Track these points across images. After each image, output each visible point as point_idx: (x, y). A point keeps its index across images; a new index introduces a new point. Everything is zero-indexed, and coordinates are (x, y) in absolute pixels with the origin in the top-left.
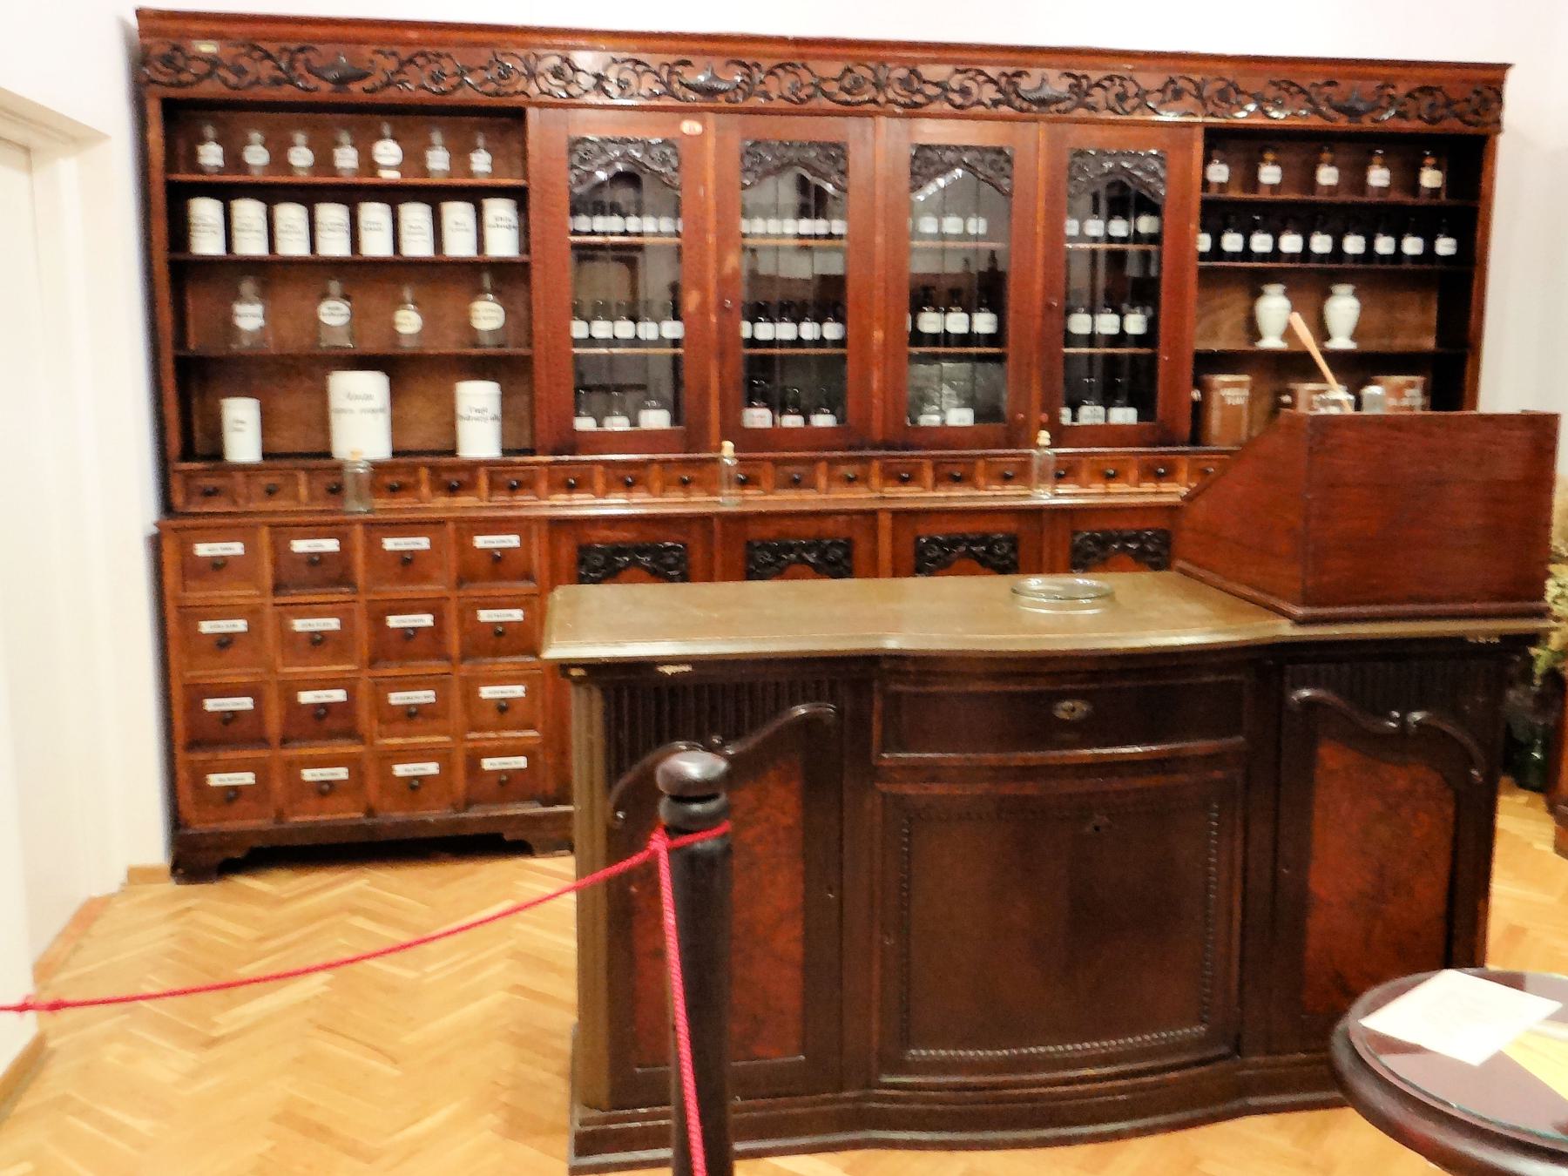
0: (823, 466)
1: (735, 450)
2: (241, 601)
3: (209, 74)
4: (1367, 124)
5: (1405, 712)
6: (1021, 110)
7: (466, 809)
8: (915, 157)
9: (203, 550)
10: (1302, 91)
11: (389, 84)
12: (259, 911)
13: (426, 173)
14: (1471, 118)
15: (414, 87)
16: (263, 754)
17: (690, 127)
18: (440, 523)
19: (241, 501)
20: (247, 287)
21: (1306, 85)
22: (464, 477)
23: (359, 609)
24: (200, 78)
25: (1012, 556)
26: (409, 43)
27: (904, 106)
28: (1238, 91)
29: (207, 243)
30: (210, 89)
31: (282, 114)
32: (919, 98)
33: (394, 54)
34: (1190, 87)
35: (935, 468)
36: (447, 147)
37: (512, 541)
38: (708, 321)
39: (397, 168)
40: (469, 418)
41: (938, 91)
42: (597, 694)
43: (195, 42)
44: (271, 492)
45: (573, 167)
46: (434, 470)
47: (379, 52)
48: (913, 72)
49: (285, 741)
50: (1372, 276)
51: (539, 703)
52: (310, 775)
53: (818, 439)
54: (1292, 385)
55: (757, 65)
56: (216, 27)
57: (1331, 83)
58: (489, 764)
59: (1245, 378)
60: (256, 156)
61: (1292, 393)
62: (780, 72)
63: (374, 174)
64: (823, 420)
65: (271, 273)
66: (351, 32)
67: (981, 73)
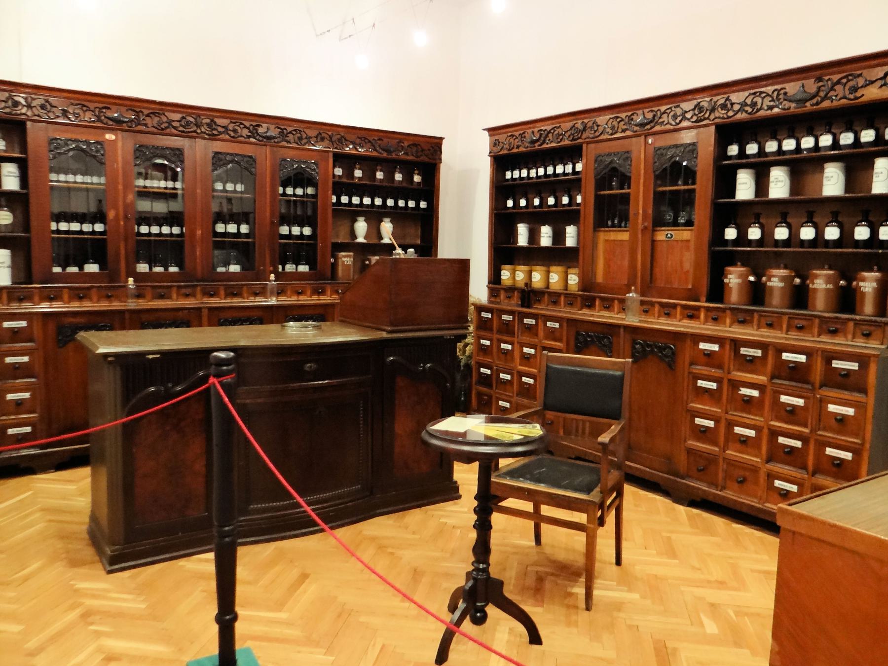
0: (174, 290)
1: (134, 281)
4: (394, 156)
5: (425, 364)
10: (370, 142)
17: (110, 136)
27: (209, 135)
32: (215, 132)
37: (24, 324)
38: (119, 224)
42: (118, 368)
48: (212, 120)
50: (396, 215)
53: (167, 276)
57: (379, 139)
59: (351, 254)
61: (370, 260)
64: (173, 269)
67: (242, 124)
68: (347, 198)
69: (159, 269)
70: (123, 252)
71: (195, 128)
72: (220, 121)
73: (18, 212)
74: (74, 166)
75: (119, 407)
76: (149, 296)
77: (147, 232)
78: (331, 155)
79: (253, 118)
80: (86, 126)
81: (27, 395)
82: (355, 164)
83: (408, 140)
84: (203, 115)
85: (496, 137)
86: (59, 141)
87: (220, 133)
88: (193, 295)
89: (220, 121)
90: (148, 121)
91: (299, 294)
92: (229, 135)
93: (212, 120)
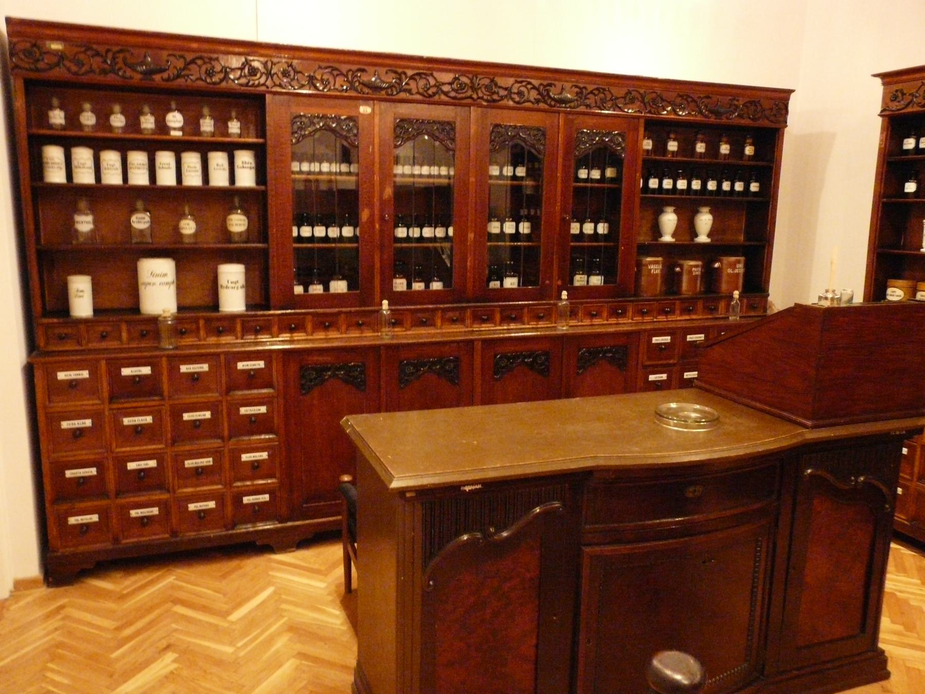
0: (439, 314)
1: (389, 305)
2: (89, 408)
3: (57, 65)
4: (724, 121)
5: (857, 477)
6: (550, 106)
7: (233, 528)
8: (493, 132)
9: (62, 376)
10: (694, 101)
11: (178, 76)
12: (110, 605)
13: (227, 135)
14: (772, 118)
15: (195, 77)
16: (104, 502)
17: (365, 109)
18: (218, 355)
19: (84, 342)
20: (83, 204)
21: (695, 97)
22: (226, 324)
23: (166, 409)
24: (51, 67)
25: (546, 363)
26: (194, 51)
27: (487, 101)
28: (663, 100)
29: (56, 176)
30: (58, 73)
31: (104, 94)
32: (495, 97)
33: (182, 57)
34: (639, 97)
35: (501, 313)
36: (212, 117)
37: (260, 364)
38: (374, 227)
39: (181, 129)
40: (227, 287)
41: (505, 93)
42: (419, 506)
43: (48, 43)
44: (103, 337)
45: (293, 133)
46: (208, 320)
47: (174, 55)
48: (492, 81)
49: (118, 494)
50: (719, 203)
51: (278, 460)
52: (134, 513)
53: (428, 296)
54: (681, 262)
55: (405, 73)
56: (60, 33)
57: (708, 97)
58: (246, 500)
59: (660, 259)
60: (88, 119)
61: (681, 266)
62: (417, 78)
63: (168, 133)
64: (437, 286)
65: (98, 195)
66: (157, 41)
67: (529, 83)
68: (671, 181)
69: (418, 286)
70: (377, 265)
71: (470, 93)
72: (501, 81)
73: (253, 213)
74: (321, 150)
75: (418, 562)
76: (408, 323)
77: (405, 235)
78: (642, 121)
79: (545, 75)
80: (336, 97)
81: (264, 455)
82: (668, 133)
83: (743, 96)
84: (482, 74)
85: (895, 87)
86: (303, 119)
87: (502, 98)
88: (461, 320)
89: (501, 81)
90: (413, 85)
91: (593, 316)
92: (513, 99)
93: (492, 81)
